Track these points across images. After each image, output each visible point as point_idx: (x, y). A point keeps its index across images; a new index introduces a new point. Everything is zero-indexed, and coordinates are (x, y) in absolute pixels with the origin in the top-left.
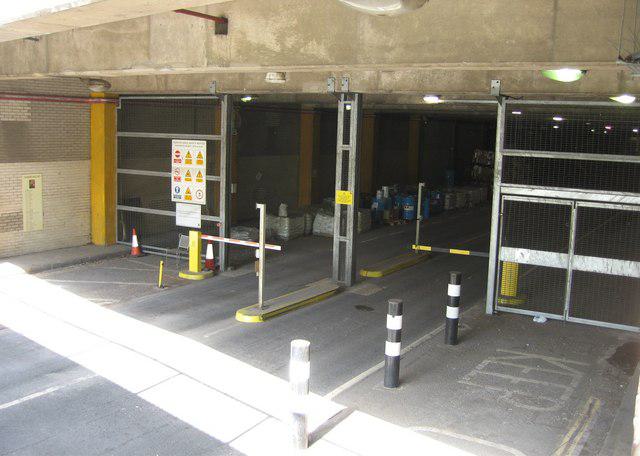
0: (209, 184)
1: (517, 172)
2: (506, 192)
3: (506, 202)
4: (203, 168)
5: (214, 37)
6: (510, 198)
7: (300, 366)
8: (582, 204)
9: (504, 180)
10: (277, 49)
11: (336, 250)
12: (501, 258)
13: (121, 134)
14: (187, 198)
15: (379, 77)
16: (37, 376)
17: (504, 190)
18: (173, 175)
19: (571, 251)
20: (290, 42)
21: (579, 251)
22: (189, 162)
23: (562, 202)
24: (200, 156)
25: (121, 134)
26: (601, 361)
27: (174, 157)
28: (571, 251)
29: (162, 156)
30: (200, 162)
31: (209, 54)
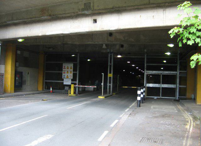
1: (149, 68)
4: (72, 70)
5: (109, 37)
8: (163, 74)
10: (124, 39)
18: (63, 72)
19: (161, 84)
20: (126, 38)
23: (174, 74)
24: (71, 67)
28: (161, 84)
30: (71, 69)
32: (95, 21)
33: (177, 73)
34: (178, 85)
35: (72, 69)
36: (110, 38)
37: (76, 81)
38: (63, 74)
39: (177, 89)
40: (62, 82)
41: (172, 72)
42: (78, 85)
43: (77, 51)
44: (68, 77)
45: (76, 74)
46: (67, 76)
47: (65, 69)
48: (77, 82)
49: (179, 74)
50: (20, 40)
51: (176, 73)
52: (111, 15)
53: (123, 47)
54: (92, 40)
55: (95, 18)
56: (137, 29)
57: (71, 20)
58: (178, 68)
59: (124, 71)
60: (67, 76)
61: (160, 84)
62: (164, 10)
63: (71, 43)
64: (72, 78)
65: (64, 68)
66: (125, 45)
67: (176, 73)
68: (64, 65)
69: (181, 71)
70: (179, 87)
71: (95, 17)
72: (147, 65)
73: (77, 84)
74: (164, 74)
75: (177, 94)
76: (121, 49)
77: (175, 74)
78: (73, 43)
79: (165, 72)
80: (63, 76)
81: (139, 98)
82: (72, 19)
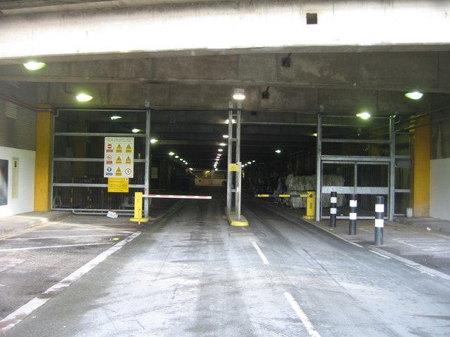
0: (136, 165)
1: (327, 150)
2: (322, 159)
3: (324, 164)
4: (131, 155)
5: (282, 68)
6: (326, 162)
7: (301, 252)
8: (359, 163)
9: (323, 153)
10: (319, 75)
11: (229, 197)
12: (323, 192)
13: (57, 134)
14: (117, 174)
15: (259, 102)
16: (150, 295)
17: (322, 159)
18: (106, 160)
19: (356, 185)
20: (326, 73)
21: (359, 185)
22: (118, 151)
23: (350, 163)
24: (129, 147)
25: (57, 134)
26: (242, 298)
27: (106, 148)
28: (356, 185)
29: (97, 149)
30: (128, 151)
31: (278, 75)
32: (312, 19)
33: (391, 160)
34: (392, 188)
35: (130, 151)
36: (285, 72)
37: (143, 183)
38: (106, 166)
39: (391, 197)
40: (103, 188)
41: (340, 158)
42: (150, 193)
43: (147, 105)
44: (120, 174)
45: (144, 164)
46: (119, 170)
47: (112, 151)
48: (146, 185)
49: (396, 163)
50: (33, 66)
51: (389, 160)
52: (90, 19)
53: (268, 98)
54: (238, 74)
55: (311, 9)
56: (392, 46)
57: (235, 12)
58: (392, 147)
59: (278, 151)
60: (119, 170)
61: (353, 186)
62: (385, 8)
63: (176, 80)
64: (132, 176)
65: (108, 151)
66: (273, 94)
67: (389, 160)
68: (108, 141)
69: (399, 157)
70: (395, 193)
71: (311, 8)
72: (323, 143)
73: (147, 191)
74: (362, 163)
75: (391, 208)
76: (264, 103)
77: (386, 163)
78: (181, 81)
79: (378, 160)
80: (106, 171)
81: (379, 223)
82: (235, 8)
